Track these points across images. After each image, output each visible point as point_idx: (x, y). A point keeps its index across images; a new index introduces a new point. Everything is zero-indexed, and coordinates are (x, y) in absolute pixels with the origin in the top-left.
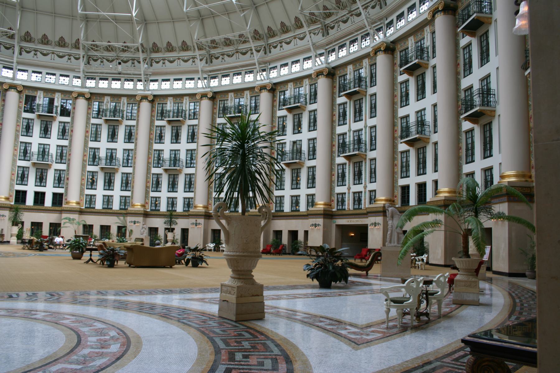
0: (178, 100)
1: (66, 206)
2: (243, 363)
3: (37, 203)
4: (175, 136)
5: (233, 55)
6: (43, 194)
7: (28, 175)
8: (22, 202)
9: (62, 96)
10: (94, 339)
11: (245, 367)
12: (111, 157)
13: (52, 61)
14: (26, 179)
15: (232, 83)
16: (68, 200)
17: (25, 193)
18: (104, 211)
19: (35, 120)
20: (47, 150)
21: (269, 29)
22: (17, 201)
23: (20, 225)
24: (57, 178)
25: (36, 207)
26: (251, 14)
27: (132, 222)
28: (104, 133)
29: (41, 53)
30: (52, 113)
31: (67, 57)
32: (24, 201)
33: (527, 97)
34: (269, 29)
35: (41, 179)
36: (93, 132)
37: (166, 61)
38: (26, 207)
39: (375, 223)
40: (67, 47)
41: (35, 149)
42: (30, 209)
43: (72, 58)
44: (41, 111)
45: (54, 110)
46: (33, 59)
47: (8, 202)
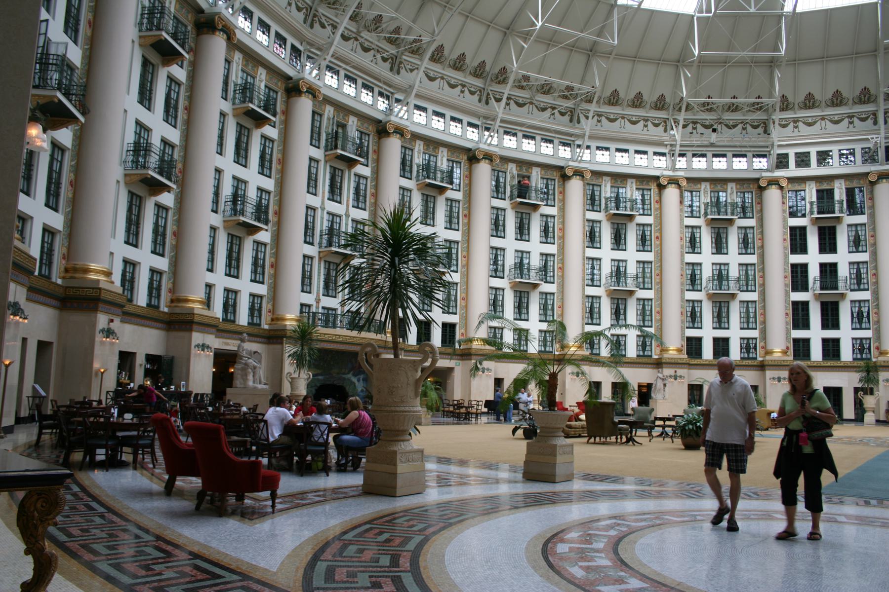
0: (619, 184)
1: (881, 359)
2: (354, 559)
3: (828, 356)
4: (620, 237)
5: (524, 104)
6: (726, 341)
7: (701, 312)
8: (804, 356)
9: (847, 183)
10: (595, 545)
11: (358, 564)
12: (721, 276)
13: (622, 130)
14: (698, 319)
15: (518, 149)
16: (769, 348)
17: (699, 340)
18: (745, 362)
19: (808, 229)
20: (622, 269)
21: (462, 57)
22: (796, 356)
23: (860, 394)
24: (855, 315)
25: (829, 363)
26: (494, 37)
27: (774, 378)
28: (706, 240)
29: (607, 118)
30: (833, 212)
31: (846, 120)
32: (726, 353)
33: (247, 144)
34: (462, 57)
35: (721, 320)
36: (863, 243)
37: (603, 119)
38: (702, 362)
39: (203, 345)
40: (845, 104)
41: (707, 272)
42: (818, 367)
43: (855, 119)
44: (729, 213)
45: (837, 207)
46: (597, 128)
47: (786, 358)
